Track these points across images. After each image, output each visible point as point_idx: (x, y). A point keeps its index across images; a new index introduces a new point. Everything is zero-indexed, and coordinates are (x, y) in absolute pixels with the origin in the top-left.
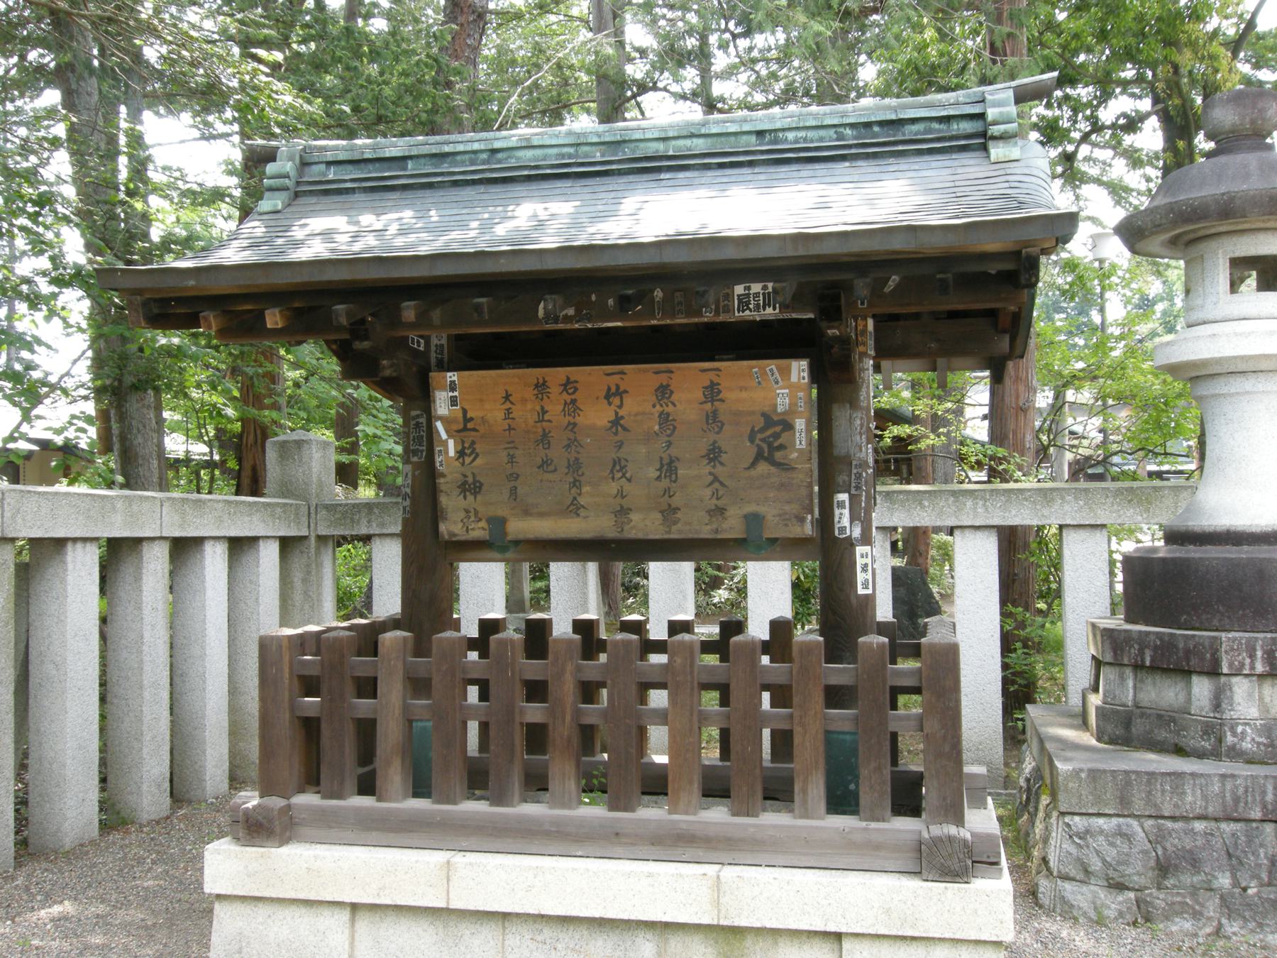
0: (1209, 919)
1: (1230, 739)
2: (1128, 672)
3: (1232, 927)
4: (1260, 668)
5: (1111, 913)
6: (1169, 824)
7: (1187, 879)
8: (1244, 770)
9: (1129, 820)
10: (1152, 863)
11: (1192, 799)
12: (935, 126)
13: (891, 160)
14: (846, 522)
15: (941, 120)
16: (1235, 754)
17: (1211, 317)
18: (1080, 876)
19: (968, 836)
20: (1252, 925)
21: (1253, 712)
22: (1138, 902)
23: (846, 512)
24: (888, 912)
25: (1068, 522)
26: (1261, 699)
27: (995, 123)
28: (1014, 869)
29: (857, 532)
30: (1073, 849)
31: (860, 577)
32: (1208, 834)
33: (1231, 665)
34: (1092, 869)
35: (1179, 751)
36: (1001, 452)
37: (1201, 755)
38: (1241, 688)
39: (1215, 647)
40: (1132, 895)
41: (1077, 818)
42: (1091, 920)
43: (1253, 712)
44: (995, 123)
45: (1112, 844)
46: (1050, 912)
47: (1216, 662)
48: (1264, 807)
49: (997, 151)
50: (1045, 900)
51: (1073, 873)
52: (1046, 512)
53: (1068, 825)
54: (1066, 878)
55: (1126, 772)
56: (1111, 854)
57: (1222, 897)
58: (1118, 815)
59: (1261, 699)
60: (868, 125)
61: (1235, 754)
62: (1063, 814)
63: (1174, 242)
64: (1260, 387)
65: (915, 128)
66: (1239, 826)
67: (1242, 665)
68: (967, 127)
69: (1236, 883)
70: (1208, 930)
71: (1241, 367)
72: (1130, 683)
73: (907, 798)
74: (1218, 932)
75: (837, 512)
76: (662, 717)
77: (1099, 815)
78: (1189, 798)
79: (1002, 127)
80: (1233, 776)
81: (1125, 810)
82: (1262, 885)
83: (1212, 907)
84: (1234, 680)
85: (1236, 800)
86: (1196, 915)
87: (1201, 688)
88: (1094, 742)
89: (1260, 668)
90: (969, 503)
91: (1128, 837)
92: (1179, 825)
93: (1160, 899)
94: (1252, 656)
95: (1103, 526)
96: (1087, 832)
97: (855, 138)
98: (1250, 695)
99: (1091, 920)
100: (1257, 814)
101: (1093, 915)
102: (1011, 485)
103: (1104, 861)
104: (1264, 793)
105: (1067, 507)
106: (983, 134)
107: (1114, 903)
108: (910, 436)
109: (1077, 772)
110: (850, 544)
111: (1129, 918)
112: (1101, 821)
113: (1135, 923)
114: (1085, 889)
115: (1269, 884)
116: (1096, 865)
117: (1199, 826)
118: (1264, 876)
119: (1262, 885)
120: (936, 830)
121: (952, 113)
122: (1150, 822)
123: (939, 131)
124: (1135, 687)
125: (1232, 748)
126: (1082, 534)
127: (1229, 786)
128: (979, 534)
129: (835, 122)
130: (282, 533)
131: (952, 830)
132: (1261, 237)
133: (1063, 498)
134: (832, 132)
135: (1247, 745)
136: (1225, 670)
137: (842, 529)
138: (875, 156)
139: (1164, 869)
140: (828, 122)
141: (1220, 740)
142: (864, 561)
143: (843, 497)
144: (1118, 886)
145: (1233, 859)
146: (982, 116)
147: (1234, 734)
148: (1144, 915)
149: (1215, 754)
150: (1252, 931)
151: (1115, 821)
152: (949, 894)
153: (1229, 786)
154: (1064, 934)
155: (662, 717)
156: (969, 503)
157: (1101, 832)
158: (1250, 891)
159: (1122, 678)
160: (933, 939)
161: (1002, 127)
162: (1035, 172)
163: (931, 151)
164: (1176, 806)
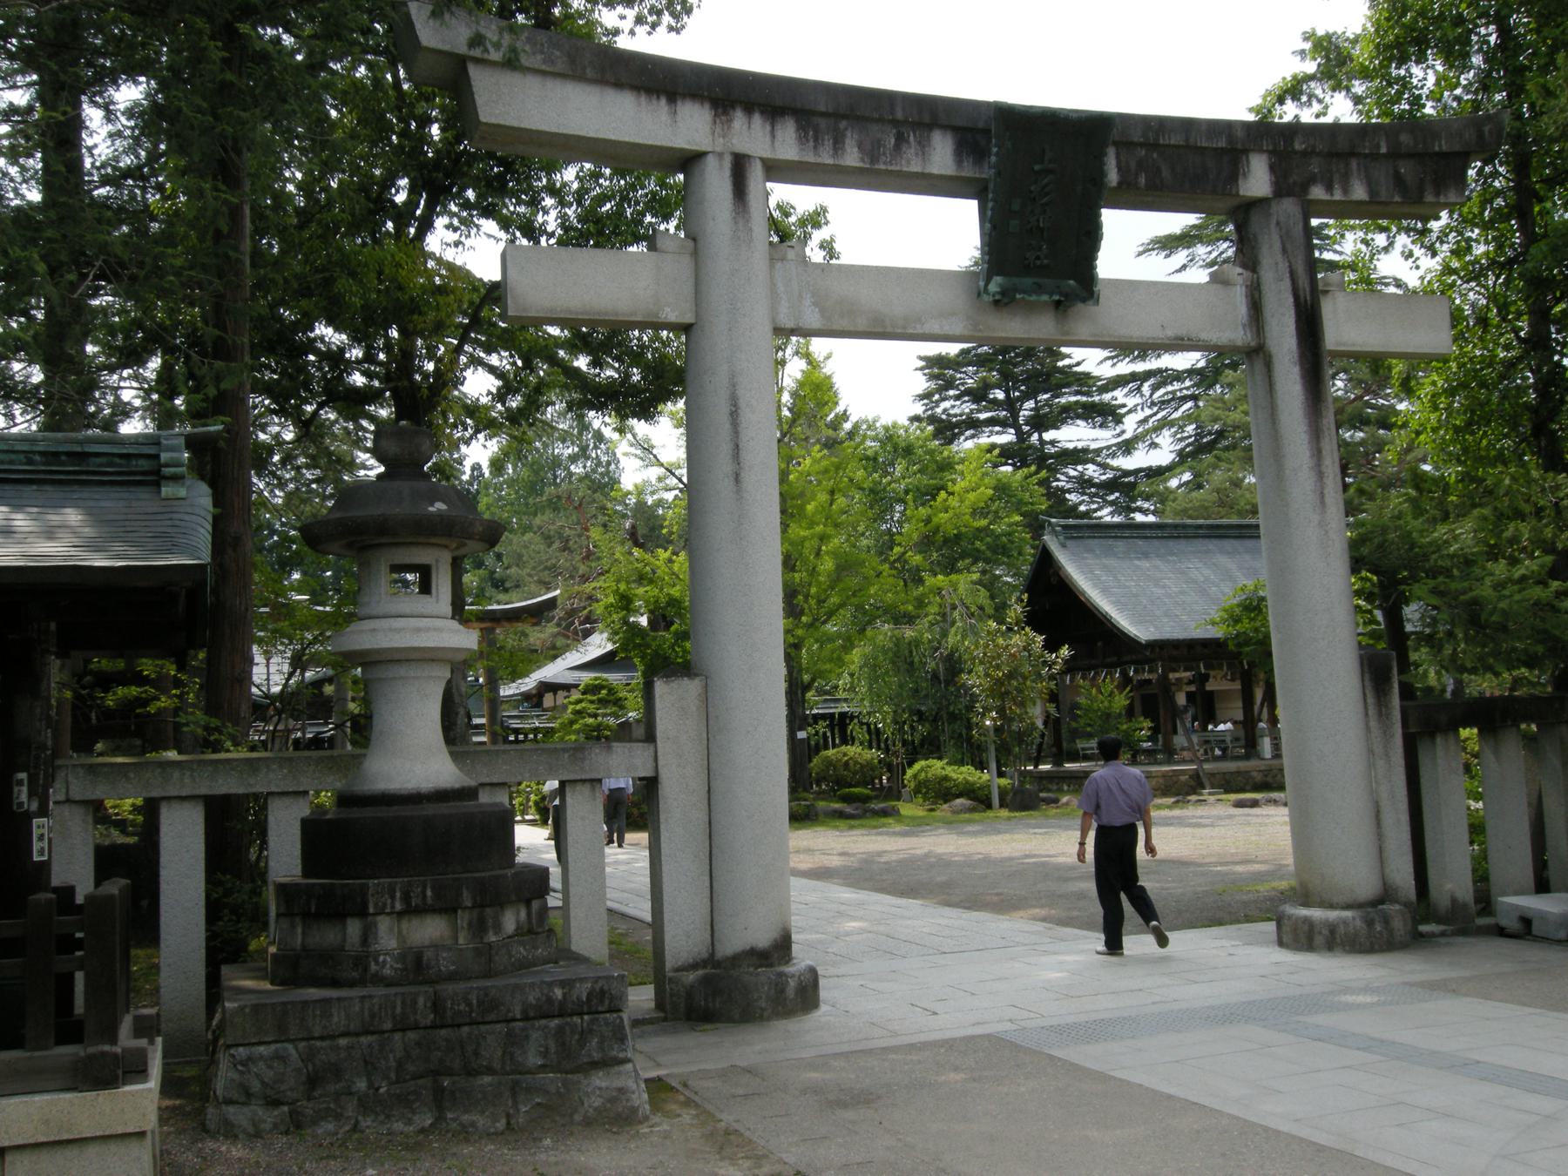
0: (348, 1118)
1: (373, 967)
2: (298, 920)
3: (366, 1122)
4: (398, 906)
5: (267, 1126)
6: (318, 1043)
7: (331, 1088)
8: (380, 991)
9: (286, 1045)
10: (304, 1078)
11: (338, 1020)
12: (117, 460)
13: (76, 488)
14: (24, 797)
15: (121, 456)
16: (378, 980)
17: (374, 612)
18: (243, 1099)
19: (119, 1050)
20: (382, 1117)
21: (393, 944)
22: (291, 1113)
23: (25, 789)
24: (47, 1122)
25: (274, 789)
26: (400, 932)
27: (167, 465)
28: (170, 1086)
29: (34, 806)
30: (236, 1076)
31: (36, 846)
32: (349, 1048)
33: (376, 905)
34: (253, 1090)
35: (335, 983)
36: (215, 722)
37: (352, 984)
38: (384, 924)
39: (364, 888)
40: (286, 1109)
41: (241, 1049)
42: (249, 1135)
43: (393, 944)
44: (167, 465)
45: (270, 1067)
46: (213, 1136)
47: (365, 905)
48: (394, 1017)
49: (166, 490)
50: (212, 1126)
51: (235, 1096)
52: (252, 781)
53: (233, 1056)
54: (229, 1102)
55: (284, 1004)
56: (269, 1075)
57: (359, 1099)
58: (276, 1042)
59: (400, 932)
60: (56, 454)
61: (378, 980)
62: (229, 1047)
63: (350, 546)
64: (412, 673)
65: (98, 460)
66: (375, 1037)
67: (385, 905)
68: (144, 464)
69: (371, 1085)
70: (347, 1128)
71: (397, 657)
72: (299, 930)
73: (70, 1032)
74: (355, 1129)
75: (16, 789)
76: (294, 52)
77: (260, 1043)
78: (336, 1019)
79: (172, 470)
80: (370, 997)
81: (282, 1036)
82: (391, 1084)
83: (350, 1109)
84: (379, 918)
85: (373, 1016)
86: (338, 1117)
87: (354, 928)
88: (269, 986)
89: (398, 906)
90: (176, 775)
91: (281, 1058)
92: (324, 1044)
93: (308, 1108)
94: (393, 898)
95: (503, 784)
96: (250, 1059)
97: (44, 464)
98: (391, 929)
99: (249, 1135)
100: (388, 1025)
101: (251, 1130)
102: (223, 756)
103: (263, 1083)
104: (394, 1007)
105: (272, 776)
106: (157, 472)
107: (268, 1117)
108: (137, 699)
109: (242, 1008)
110: (27, 817)
111: (282, 1128)
112: (262, 1048)
113: (287, 1133)
114: (246, 1109)
115: (398, 1082)
116: (256, 1086)
117: (343, 1042)
118: (393, 1076)
119: (391, 1084)
120: (91, 1050)
121: (131, 451)
122: (302, 1045)
123: (120, 465)
124: (303, 933)
125: (376, 975)
126: (287, 801)
127: (367, 1005)
128: (186, 805)
129: (25, 448)
130: (204, 791)
131: (107, 1048)
132: (414, 550)
133: (268, 767)
134: (22, 457)
135: (387, 971)
136: (371, 910)
137: (21, 804)
138: (61, 482)
139: (313, 1082)
140: (18, 447)
141: (366, 969)
142: (40, 831)
143: (23, 776)
144: (274, 1103)
145: (369, 1065)
146: (157, 457)
147: (377, 962)
148: (296, 1124)
149: (360, 982)
150: (382, 1123)
151: (273, 1047)
152: (101, 1099)
153: (367, 1005)
154: (224, 1148)
155: (294, 52)
156: (176, 775)
157: (261, 1057)
158: (382, 1090)
159: (293, 927)
160: (86, 1139)
161: (172, 470)
162: (197, 511)
163: (112, 483)
164: (325, 1027)
